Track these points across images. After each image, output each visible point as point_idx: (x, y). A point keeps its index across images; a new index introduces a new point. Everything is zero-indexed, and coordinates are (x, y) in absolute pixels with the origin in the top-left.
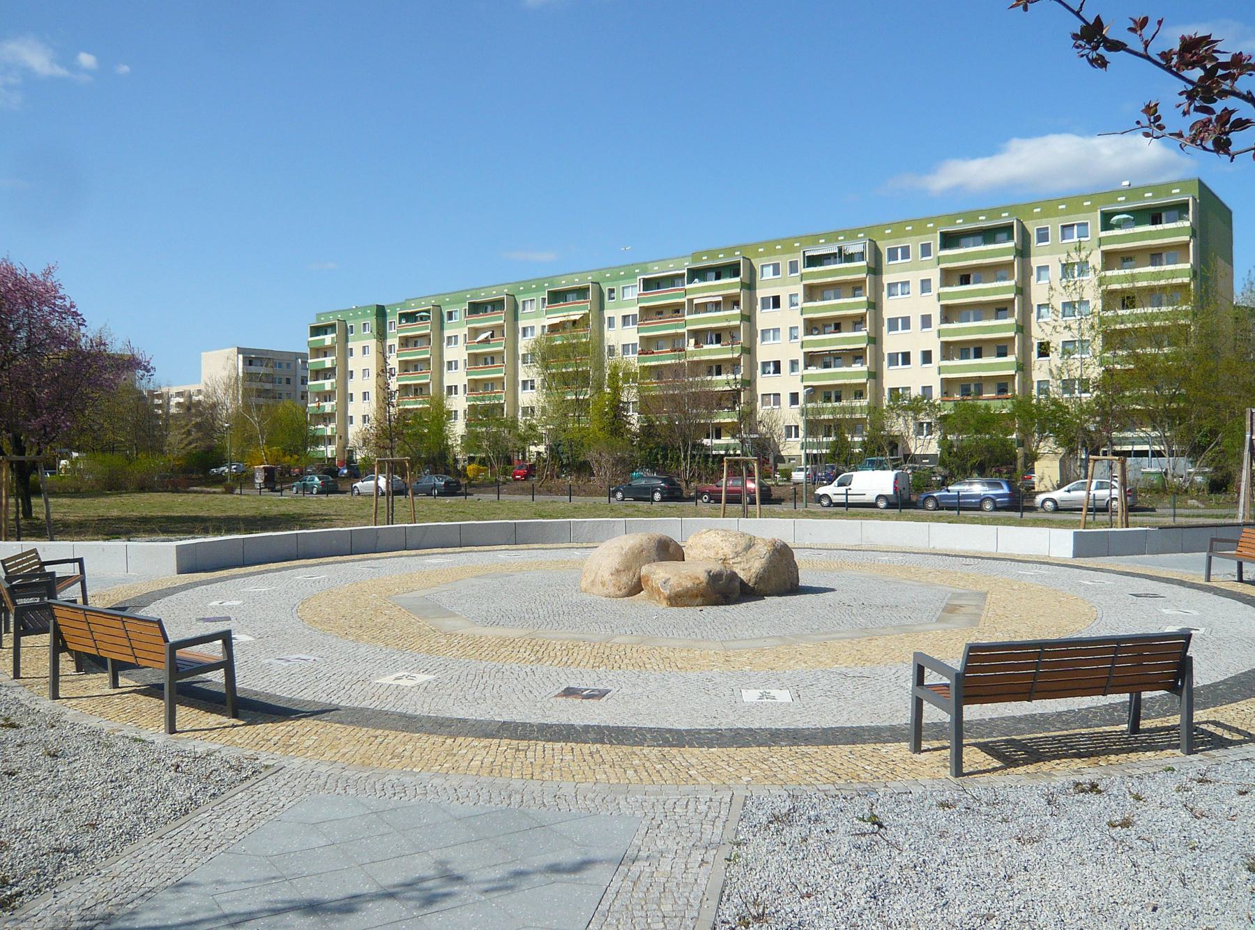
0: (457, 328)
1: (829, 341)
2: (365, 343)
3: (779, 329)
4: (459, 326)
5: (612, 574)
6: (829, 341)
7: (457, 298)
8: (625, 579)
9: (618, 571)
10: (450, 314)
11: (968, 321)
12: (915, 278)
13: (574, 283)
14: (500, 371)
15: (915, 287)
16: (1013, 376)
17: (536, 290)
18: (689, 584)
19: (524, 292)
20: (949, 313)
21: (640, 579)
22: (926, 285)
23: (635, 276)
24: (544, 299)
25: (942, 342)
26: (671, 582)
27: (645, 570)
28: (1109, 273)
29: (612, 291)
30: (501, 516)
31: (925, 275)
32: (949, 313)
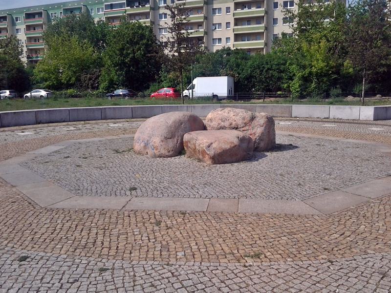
0: (21, 26)
1: (245, 29)
2: (228, 5)
3: (221, 23)
4: (21, 24)
5: (162, 141)
6: (245, 29)
7: (20, 11)
8: (171, 144)
9: (166, 138)
10: (17, 18)
11: (245, 25)
12: (224, 6)
13: (75, 5)
14: (42, 45)
15: (224, 10)
16: (263, 48)
17: (57, 8)
18: (228, 147)
19: (51, 9)
20: (238, 21)
21: (182, 143)
22: (228, 10)
23: (102, 3)
24: (61, 13)
25: (235, 34)
26: (214, 145)
27: (186, 137)
28: (236, 12)
29: (17, 18)
30: (387, 103)
31: (228, 5)
32: (238, 21)
